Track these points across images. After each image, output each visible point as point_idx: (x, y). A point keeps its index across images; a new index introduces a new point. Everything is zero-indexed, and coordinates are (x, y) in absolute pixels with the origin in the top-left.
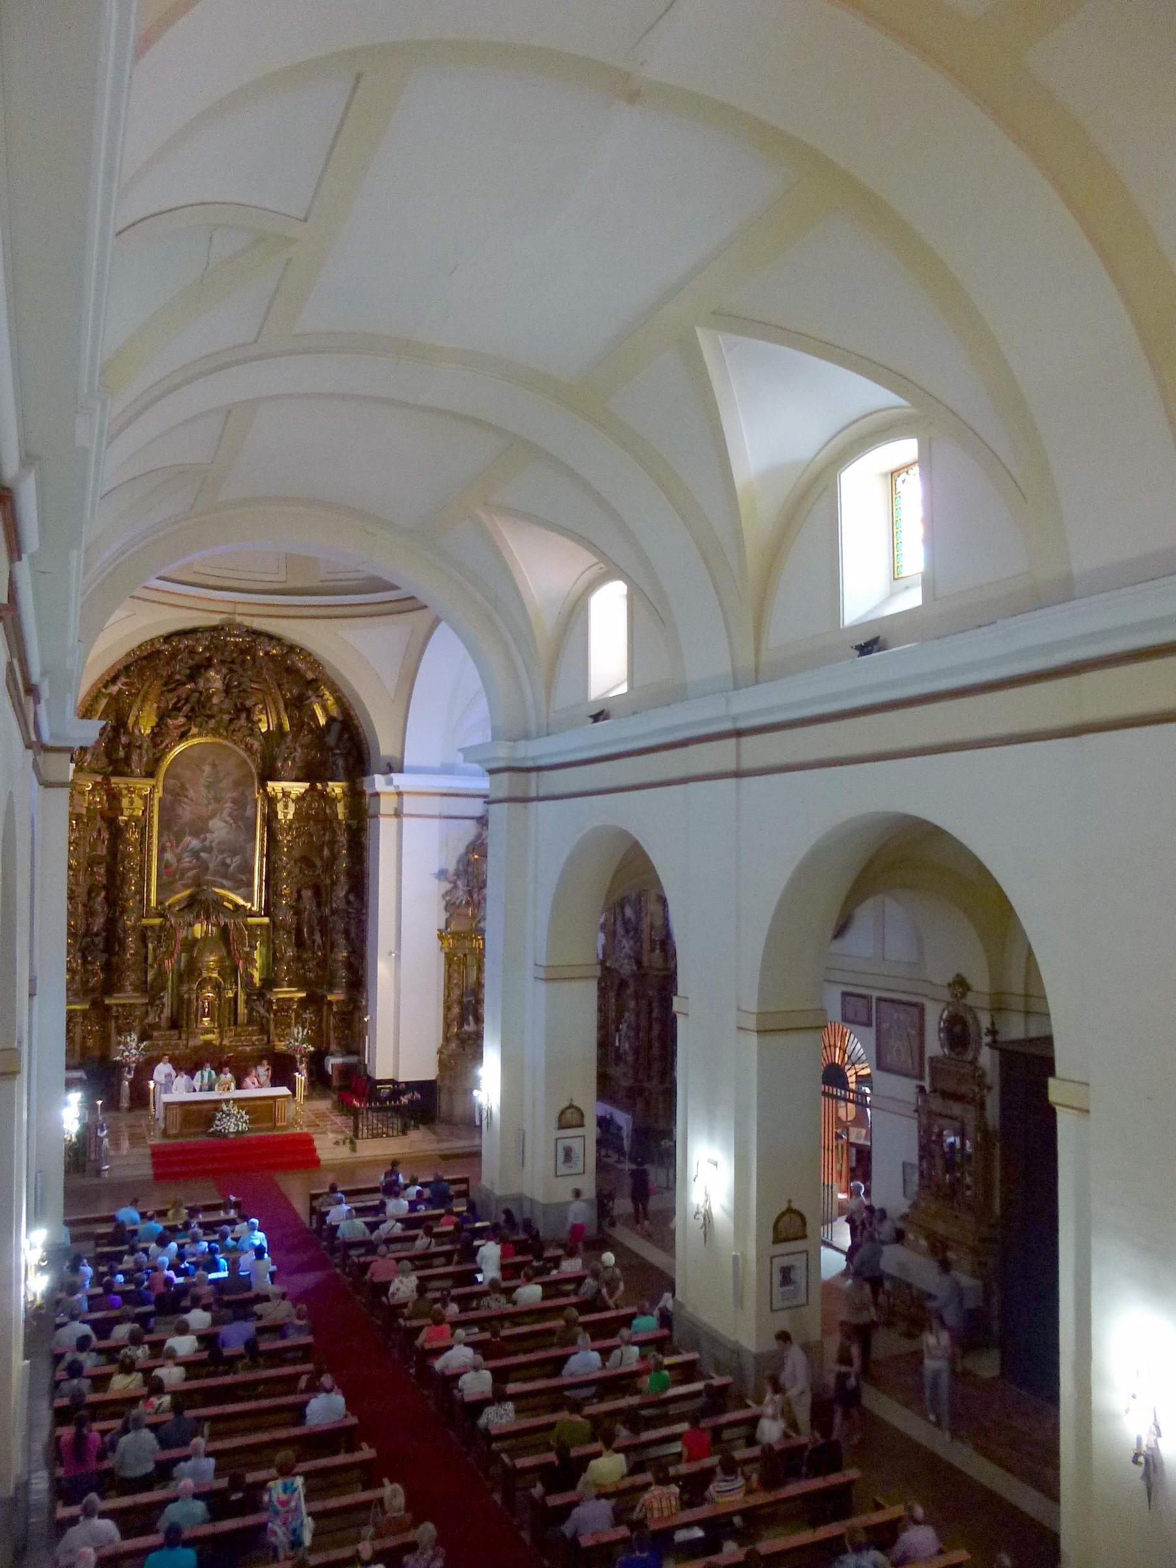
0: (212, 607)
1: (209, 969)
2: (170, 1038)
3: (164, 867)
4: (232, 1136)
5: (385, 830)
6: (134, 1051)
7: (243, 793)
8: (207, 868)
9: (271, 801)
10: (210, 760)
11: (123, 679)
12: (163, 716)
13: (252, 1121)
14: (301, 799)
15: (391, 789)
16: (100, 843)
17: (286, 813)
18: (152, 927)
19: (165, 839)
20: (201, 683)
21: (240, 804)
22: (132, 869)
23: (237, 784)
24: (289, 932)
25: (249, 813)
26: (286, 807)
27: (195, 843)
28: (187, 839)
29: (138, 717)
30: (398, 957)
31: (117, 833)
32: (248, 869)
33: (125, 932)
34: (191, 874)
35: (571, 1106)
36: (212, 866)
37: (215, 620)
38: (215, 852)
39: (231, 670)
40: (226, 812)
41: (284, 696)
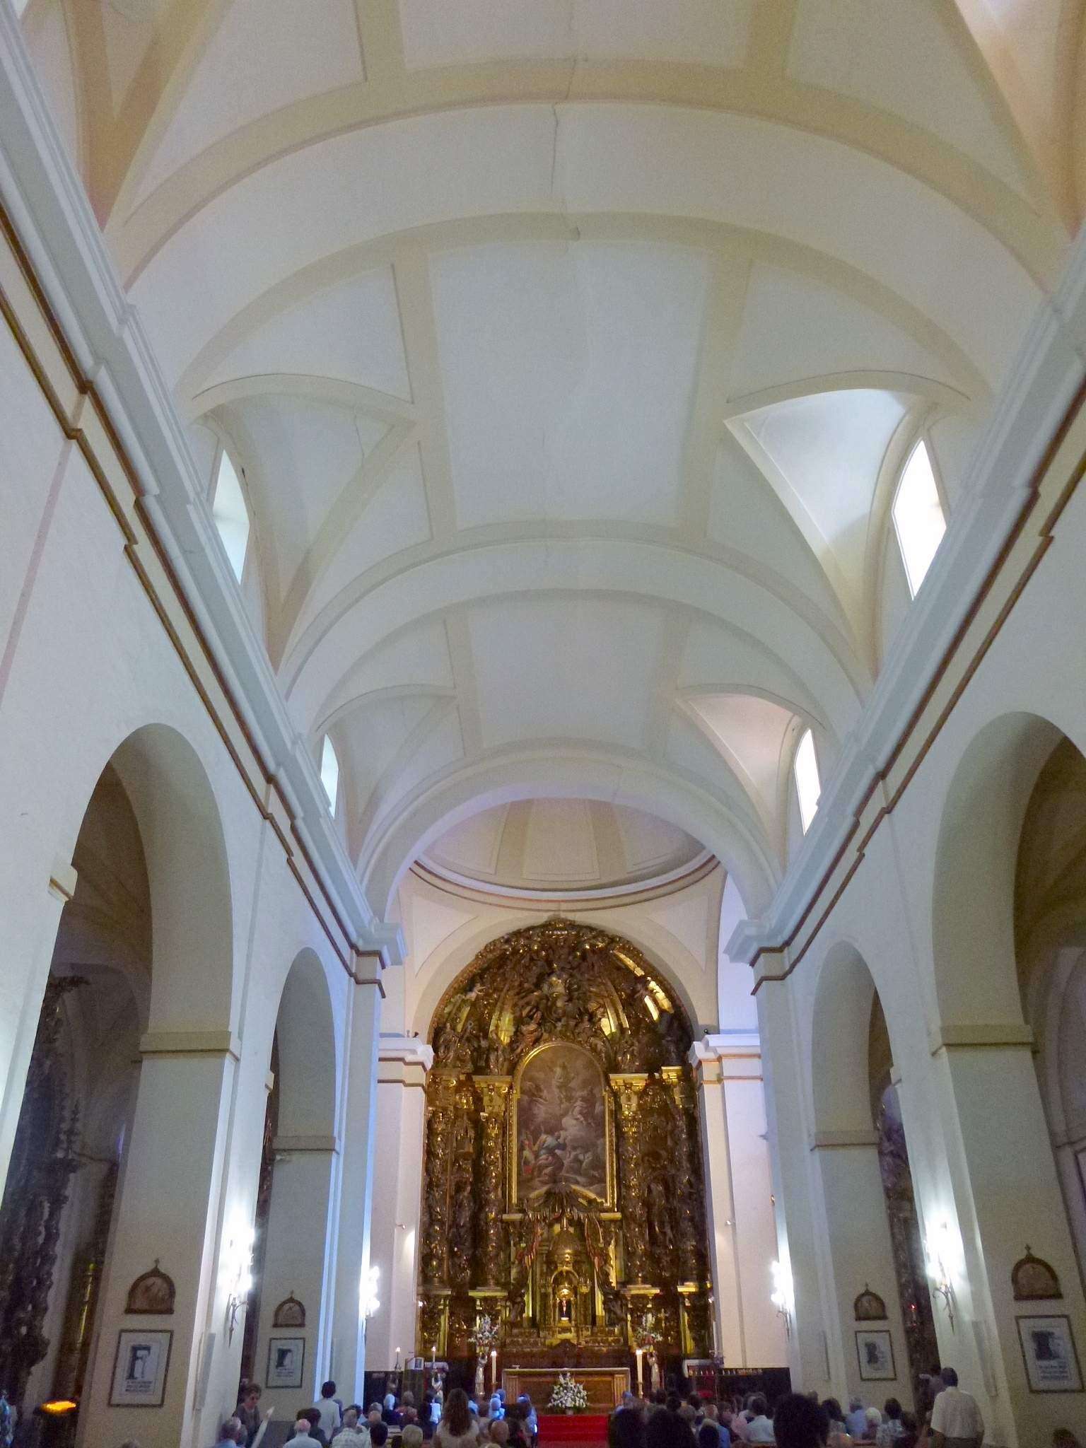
0: (540, 906)
1: (564, 1262)
2: (530, 1334)
3: (522, 1162)
4: (570, 1413)
5: (710, 1095)
6: (487, 1334)
7: (591, 1091)
8: (563, 1164)
9: (616, 1095)
10: (560, 1062)
11: (478, 987)
12: (519, 1022)
13: (589, 1399)
14: (642, 1094)
15: (712, 1055)
16: (467, 1142)
17: (629, 1108)
18: (513, 1223)
19: (523, 1137)
20: (545, 987)
21: (590, 1101)
22: (493, 1163)
23: (585, 1084)
24: (640, 1226)
25: (598, 1108)
26: (629, 1099)
27: (549, 1140)
28: (543, 1137)
29: (497, 1027)
30: (734, 1225)
31: (479, 1128)
32: (598, 1165)
33: (486, 1224)
34: (548, 1170)
35: (867, 1293)
36: (566, 1162)
37: (543, 918)
38: (569, 1148)
39: (571, 975)
40: (577, 1109)
41: (620, 996)
